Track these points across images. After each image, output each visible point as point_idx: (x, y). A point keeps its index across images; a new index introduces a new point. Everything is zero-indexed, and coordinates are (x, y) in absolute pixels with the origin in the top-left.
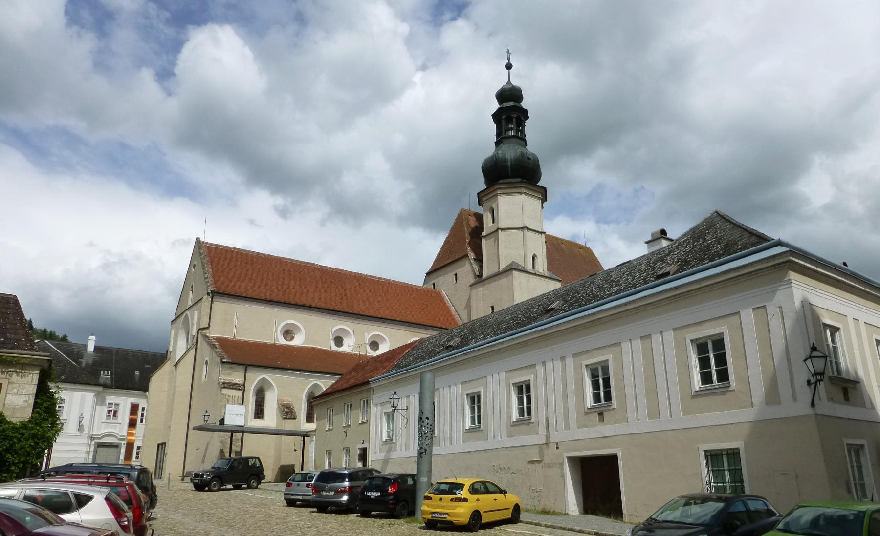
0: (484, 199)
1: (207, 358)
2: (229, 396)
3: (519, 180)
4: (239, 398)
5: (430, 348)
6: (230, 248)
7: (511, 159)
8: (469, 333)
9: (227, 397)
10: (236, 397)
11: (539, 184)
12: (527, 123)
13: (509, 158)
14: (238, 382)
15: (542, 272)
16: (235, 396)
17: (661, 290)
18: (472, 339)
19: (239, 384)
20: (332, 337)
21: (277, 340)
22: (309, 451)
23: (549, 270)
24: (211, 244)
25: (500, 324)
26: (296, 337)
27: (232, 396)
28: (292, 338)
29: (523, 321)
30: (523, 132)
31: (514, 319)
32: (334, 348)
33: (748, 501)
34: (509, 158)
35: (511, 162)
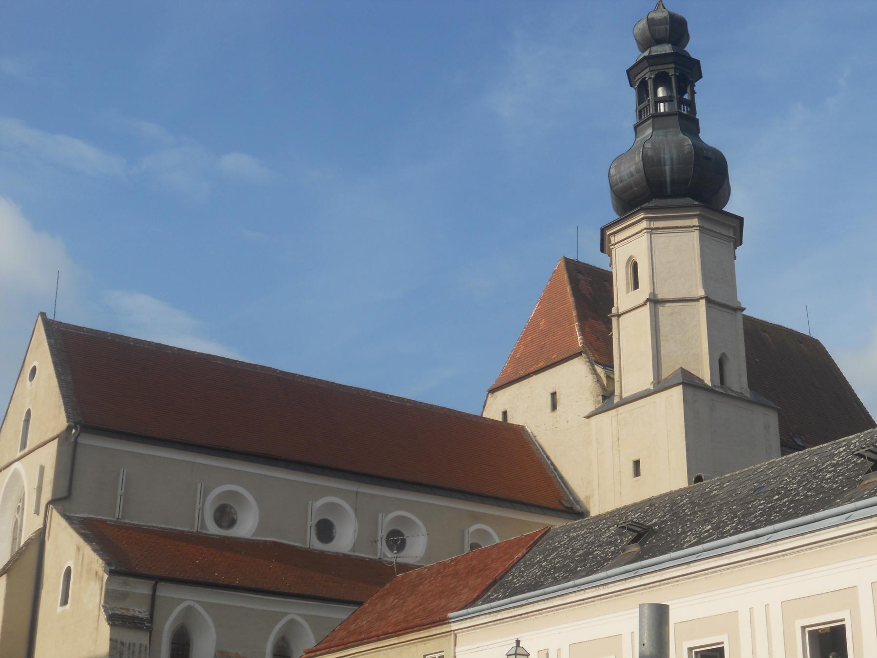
0: (613, 240)
1: (70, 563)
2: (122, 644)
3: (688, 201)
4: (143, 649)
5: (578, 550)
6: (105, 333)
7: (672, 159)
8: (671, 520)
9: (119, 646)
10: (137, 647)
11: (726, 209)
12: (699, 86)
13: (667, 157)
14: (140, 616)
15: (739, 391)
16: (134, 645)
17: (41, 508)
18: (684, 532)
19: (142, 619)
20: (312, 522)
21: (203, 525)
22: (63, 611)
23: (751, 385)
24: (67, 326)
25: (749, 503)
26: (240, 517)
27: (130, 645)
28: (232, 523)
29: (806, 496)
30: (691, 104)
31: (779, 493)
32: (318, 545)
33: (154, 582)
34: (667, 157)
35: (672, 164)
